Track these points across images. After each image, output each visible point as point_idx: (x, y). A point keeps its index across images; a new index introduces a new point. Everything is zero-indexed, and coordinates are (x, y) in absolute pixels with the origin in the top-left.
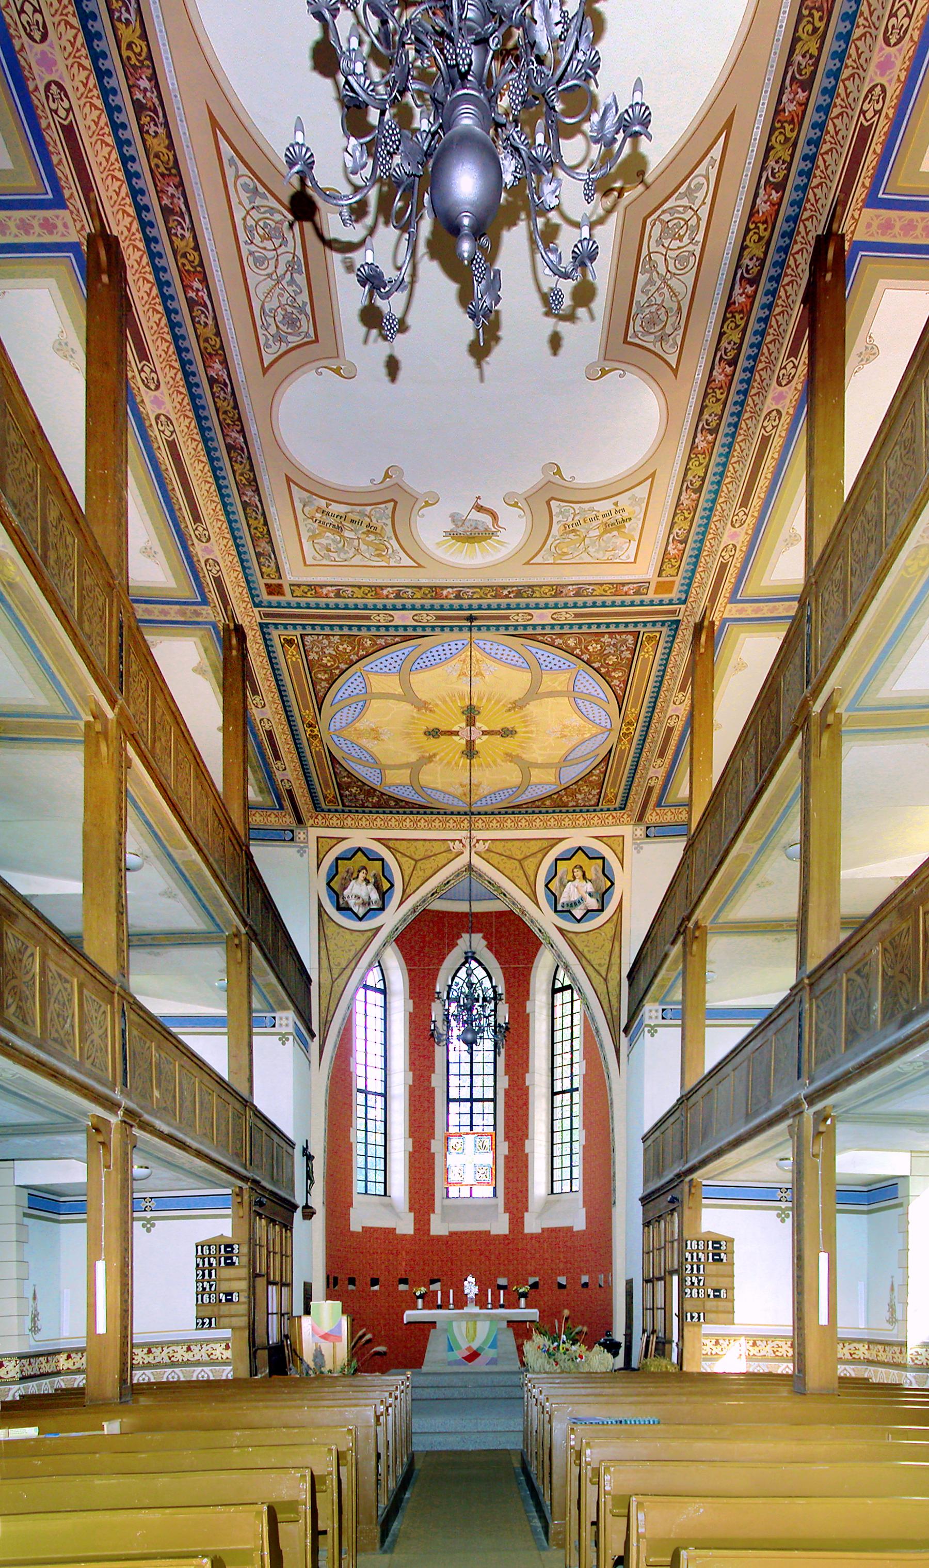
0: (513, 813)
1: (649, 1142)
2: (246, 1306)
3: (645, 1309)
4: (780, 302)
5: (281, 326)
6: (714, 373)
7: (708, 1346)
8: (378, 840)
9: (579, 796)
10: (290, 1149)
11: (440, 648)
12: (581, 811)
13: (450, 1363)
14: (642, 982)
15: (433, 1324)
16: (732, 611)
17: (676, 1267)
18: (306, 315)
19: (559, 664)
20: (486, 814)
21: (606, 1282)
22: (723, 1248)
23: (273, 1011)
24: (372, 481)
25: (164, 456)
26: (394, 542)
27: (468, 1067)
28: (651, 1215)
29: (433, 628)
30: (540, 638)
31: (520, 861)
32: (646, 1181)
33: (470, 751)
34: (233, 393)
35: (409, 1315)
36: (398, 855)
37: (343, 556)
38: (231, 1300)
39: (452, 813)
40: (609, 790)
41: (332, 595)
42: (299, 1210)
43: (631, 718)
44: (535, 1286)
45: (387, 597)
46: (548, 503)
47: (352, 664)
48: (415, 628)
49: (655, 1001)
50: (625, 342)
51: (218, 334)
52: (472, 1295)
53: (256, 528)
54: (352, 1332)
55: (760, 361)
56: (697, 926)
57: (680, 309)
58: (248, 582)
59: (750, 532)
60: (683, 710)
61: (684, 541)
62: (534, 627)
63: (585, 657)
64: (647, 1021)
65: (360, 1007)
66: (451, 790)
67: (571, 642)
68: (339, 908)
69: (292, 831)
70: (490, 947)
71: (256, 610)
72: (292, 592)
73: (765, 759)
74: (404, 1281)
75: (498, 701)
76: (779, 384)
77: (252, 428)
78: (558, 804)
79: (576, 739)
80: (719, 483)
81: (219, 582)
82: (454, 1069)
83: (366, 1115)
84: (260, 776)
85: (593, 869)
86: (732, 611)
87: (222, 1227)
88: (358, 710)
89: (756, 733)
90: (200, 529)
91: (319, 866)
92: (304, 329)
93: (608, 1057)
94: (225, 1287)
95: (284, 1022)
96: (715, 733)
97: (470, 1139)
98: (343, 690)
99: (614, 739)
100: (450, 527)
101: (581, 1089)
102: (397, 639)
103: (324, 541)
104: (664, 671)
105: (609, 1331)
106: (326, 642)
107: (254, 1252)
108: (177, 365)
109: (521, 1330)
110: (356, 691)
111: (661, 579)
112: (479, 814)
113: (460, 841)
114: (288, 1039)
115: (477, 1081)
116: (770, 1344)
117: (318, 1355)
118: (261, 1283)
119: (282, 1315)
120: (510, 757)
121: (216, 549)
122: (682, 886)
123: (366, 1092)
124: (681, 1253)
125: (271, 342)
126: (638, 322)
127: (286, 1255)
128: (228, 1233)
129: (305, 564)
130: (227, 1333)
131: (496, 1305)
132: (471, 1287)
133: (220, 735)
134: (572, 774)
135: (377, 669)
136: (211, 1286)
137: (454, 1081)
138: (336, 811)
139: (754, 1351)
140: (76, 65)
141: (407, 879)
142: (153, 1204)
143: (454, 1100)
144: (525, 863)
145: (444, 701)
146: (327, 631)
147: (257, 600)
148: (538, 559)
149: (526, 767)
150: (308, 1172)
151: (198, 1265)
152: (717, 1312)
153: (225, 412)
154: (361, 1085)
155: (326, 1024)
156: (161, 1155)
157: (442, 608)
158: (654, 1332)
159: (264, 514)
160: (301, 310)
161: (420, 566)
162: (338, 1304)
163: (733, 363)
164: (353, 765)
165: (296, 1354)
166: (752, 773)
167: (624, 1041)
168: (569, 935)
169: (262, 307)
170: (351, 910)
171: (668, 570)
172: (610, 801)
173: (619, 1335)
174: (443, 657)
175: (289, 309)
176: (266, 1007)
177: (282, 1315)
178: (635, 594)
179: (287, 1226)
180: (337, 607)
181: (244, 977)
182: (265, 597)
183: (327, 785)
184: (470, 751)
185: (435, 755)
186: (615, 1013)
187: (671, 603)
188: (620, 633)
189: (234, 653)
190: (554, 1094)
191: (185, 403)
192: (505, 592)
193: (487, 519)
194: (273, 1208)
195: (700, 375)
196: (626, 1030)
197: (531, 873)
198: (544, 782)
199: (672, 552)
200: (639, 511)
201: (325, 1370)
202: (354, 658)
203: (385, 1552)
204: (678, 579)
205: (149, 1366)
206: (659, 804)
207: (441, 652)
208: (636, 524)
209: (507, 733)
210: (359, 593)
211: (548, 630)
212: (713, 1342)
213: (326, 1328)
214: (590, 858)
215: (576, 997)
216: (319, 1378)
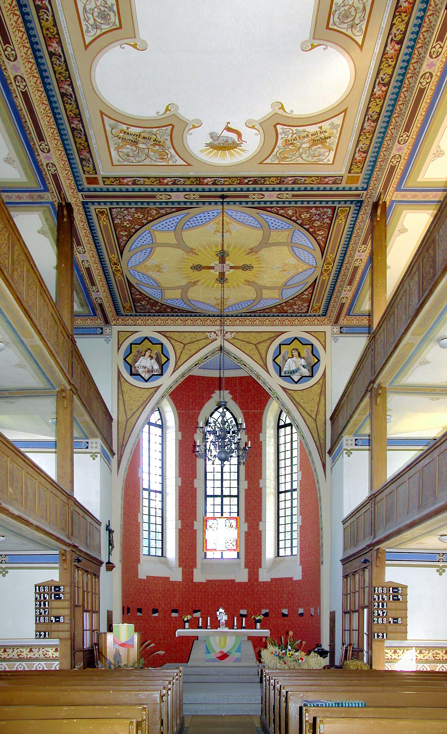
0: (250, 316)
1: (348, 524)
2: (69, 625)
3: (344, 630)
4: (431, 8)
5: (97, 19)
6: (387, 49)
7: (389, 654)
10: (98, 526)
11: (202, 215)
12: (296, 316)
13: (207, 661)
14: (341, 421)
15: (197, 638)
16: (398, 196)
17: (366, 603)
18: (114, 11)
19: (282, 226)
20: (232, 316)
21: (316, 612)
22: (400, 592)
23: (87, 438)
24: (157, 113)
25: (20, 102)
26: (172, 150)
27: (221, 475)
28: (349, 571)
29: (197, 203)
30: (270, 209)
31: (255, 345)
32: (345, 549)
33: (222, 278)
34: (65, 61)
35: (179, 632)
36: (172, 341)
37: (138, 159)
38: (59, 621)
39: (209, 316)
40: (314, 304)
41: (130, 183)
42: (104, 565)
43: (330, 260)
44: (266, 615)
45: (167, 184)
46: (275, 126)
47: (143, 225)
48: (185, 203)
49: (350, 434)
50: (327, 28)
51: (55, 25)
52: (223, 621)
53: (80, 144)
54: (142, 643)
55: (418, 43)
56: (380, 387)
57: (364, 9)
58: (74, 176)
59: (410, 147)
60: (365, 256)
61: (366, 152)
62: (265, 202)
63: (299, 222)
64: (345, 447)
65: (145, 436)
66: (209, 302)
67: (290, 212)
68: (131, 374)
69: (102, 329)
70: (234, 399)
71: (80, 194)
72: (104, 182)
73: (425, 283)
74: (175, 611)
75: (241, 248)
76: (431, 57)
77: (78, 83)
78: (282, 311)
79: (293, 273)
80: (389, 117)
81: (55, 177)
82: (209, 476)
83: (150, 505)
84: (81, 296)
85: (305, 351)
86: (398, 196)
87: (53, 575)
88: (147, 254)
89: (418, 268)
90: (22, 87)
91: (119, 349)
92: (113, 20)
93: (317, 470)
94: (55, 612)
95: (94, 445)
96: (388, 271)
97: (222, 521)
98: (137, 242)
99: (318, 273)
100: (209, 140)
101: (298, 490)
102: (174, 210)
103: (125, 150)
104: (352, 232)
105: (319, 645)
106: (126, 212)
107: (74, 591)
108: (28, 45)
109: (259, 644)
110: (145, 242)
111: (350, 175)
112: (227, 316)
113: (215, 332)
114: (97, 456)
115: (226, 484)
116: (431, 652)
117: (117, 655)
118: (79, 610)
119: (93, 631)
120: (249, 283)
121: (54, 157)
122: (368, 363)
123: (149, 490)
124: (371, 595)
125: (90, 29)
126: (336, 16)
127: (96, 593)
128: (57, 578)
129: (113, 165)
130: (56, 642)
132: (222, 616)
133: (55, 271)
134: (289, 294)
135: (160, 228)
136: (45, 612)
137: (209, 484)
138: (131, 315)
139: (420, 656)
140: (17, 31)
141: (178, 355)
142: (7, 559)
143: (235, 496)
144: (259, 346)
145: (205, 249)
146: (127, 206)
148: (268, 161)
149: (259, 289)
150: (109, 541)
151: (36, 598)
152: (395, 632)
153: (60, 73)
154: (146, 486)
155: (122, 447)
156: (12, 529)
157: (204, 190)
158: (350, 645)
159: (85, 135)
160: (111, 9)
161: (189, 165)
163: (400, 42)
164: (146, 289)
165: (102, 655)
166: (416, 292)
167: (328, 459)
168: (290, 392)
169: (85, 8)
170: (140, 375)
171: (355, 169)
172: (316, 310)
173: (326, 646)
174: (204, 221)
175: (103, 9)
176: (82, 436)
177: (93, 631)
178: (333, 183)
179: (97, 575)
180: (134, 191)
181: (68, 418)
182: (86, 186)
183: (125, 298)
184: (222, 278)
185: (198, 281)
186: (322, 441)
189: (65, 220)
190: (279, 493)
191: (47, 109)
192: (246, 181)
193: (235, 136)
194: (84, 563)
195: (378, 49)
196: (330, 452)
197: (263, 352)
198: (271, 298)
199: (358, 158)
200: (336, 133)
201: (122, 664)
202: (145, 222)
204: (362, 176)
206: (348, 314)
207: (203, 218)
208: (334, 141)
209: (246, 268)
210: (148, 181)
211: (275, 205)
212: (393, 651)
213: (123, 639)
214: (303, 344)
216: (118, 670)
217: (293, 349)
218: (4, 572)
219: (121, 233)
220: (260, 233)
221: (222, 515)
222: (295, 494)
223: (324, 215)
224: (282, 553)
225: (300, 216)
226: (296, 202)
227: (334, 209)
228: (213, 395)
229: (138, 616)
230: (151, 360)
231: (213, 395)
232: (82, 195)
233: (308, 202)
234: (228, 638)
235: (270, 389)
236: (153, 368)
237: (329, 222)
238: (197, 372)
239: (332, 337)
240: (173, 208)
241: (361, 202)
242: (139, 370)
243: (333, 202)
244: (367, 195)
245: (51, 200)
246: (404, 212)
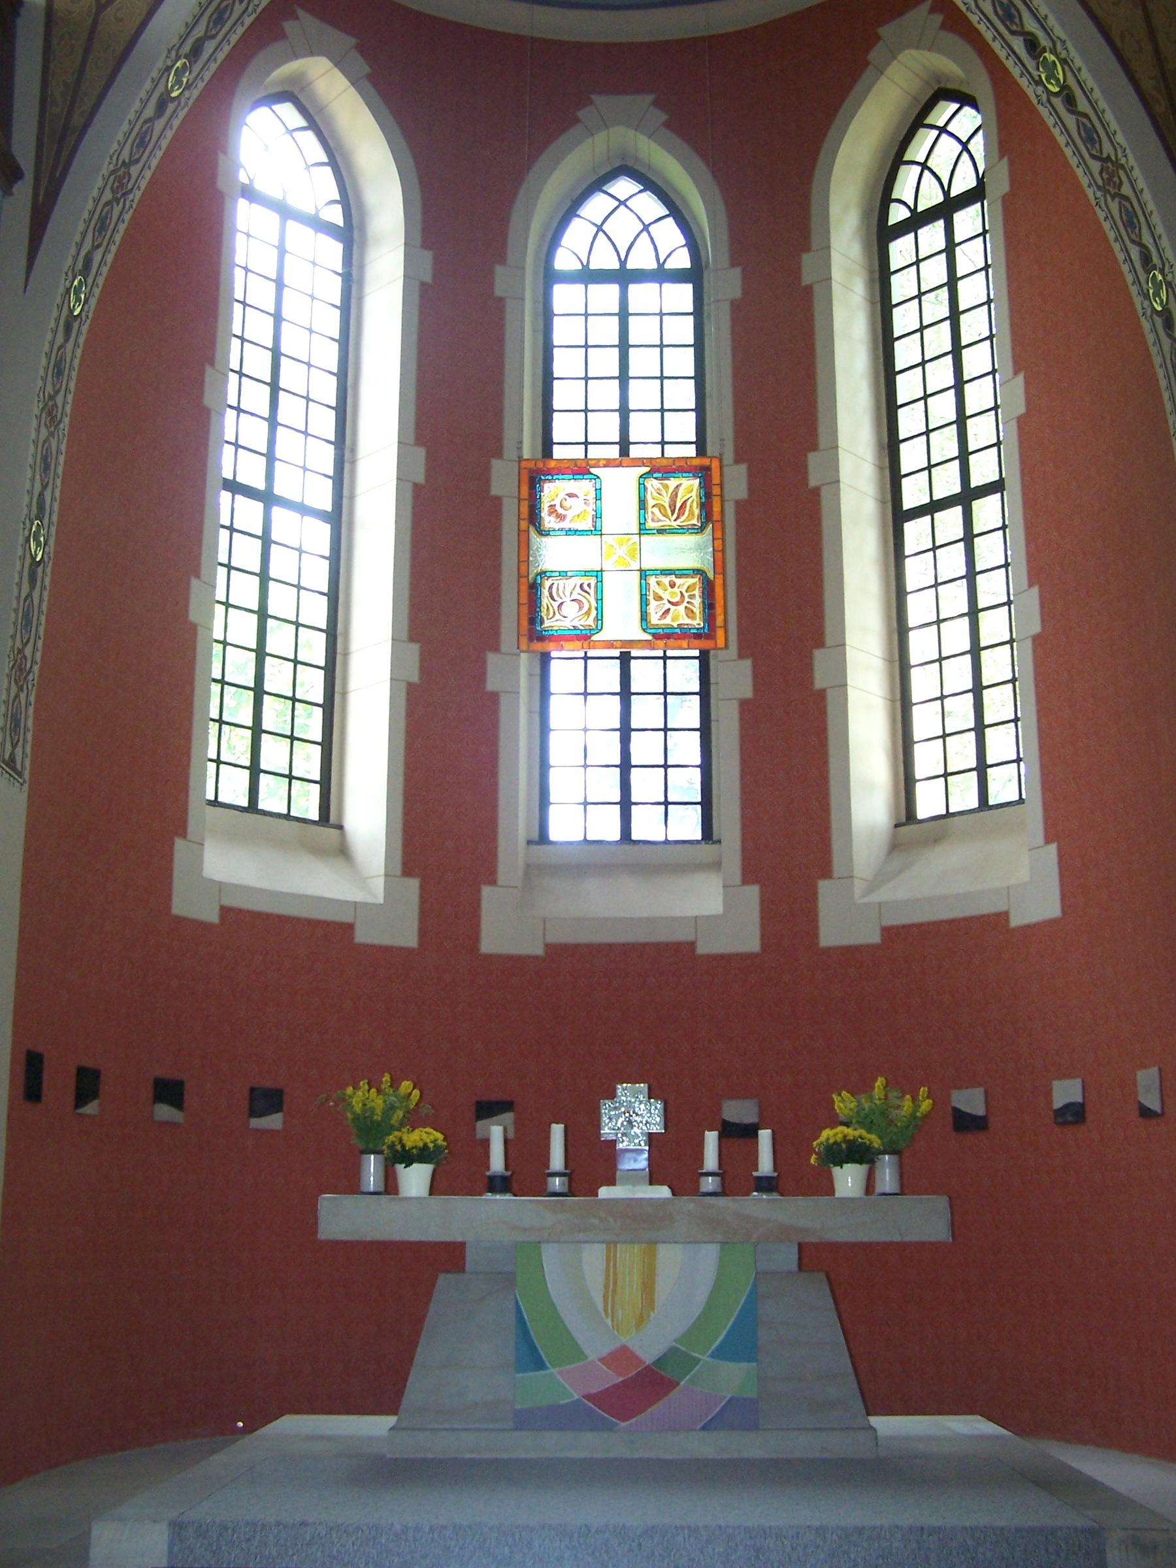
13: (525, 1420)
15: (450, 1256)
131: (737, 1178)
132: (633, 1118)
221: (624, 452)
222: (987, 511)
224: (929, 803)
229: (163, 1124)
234: (670, 1257)
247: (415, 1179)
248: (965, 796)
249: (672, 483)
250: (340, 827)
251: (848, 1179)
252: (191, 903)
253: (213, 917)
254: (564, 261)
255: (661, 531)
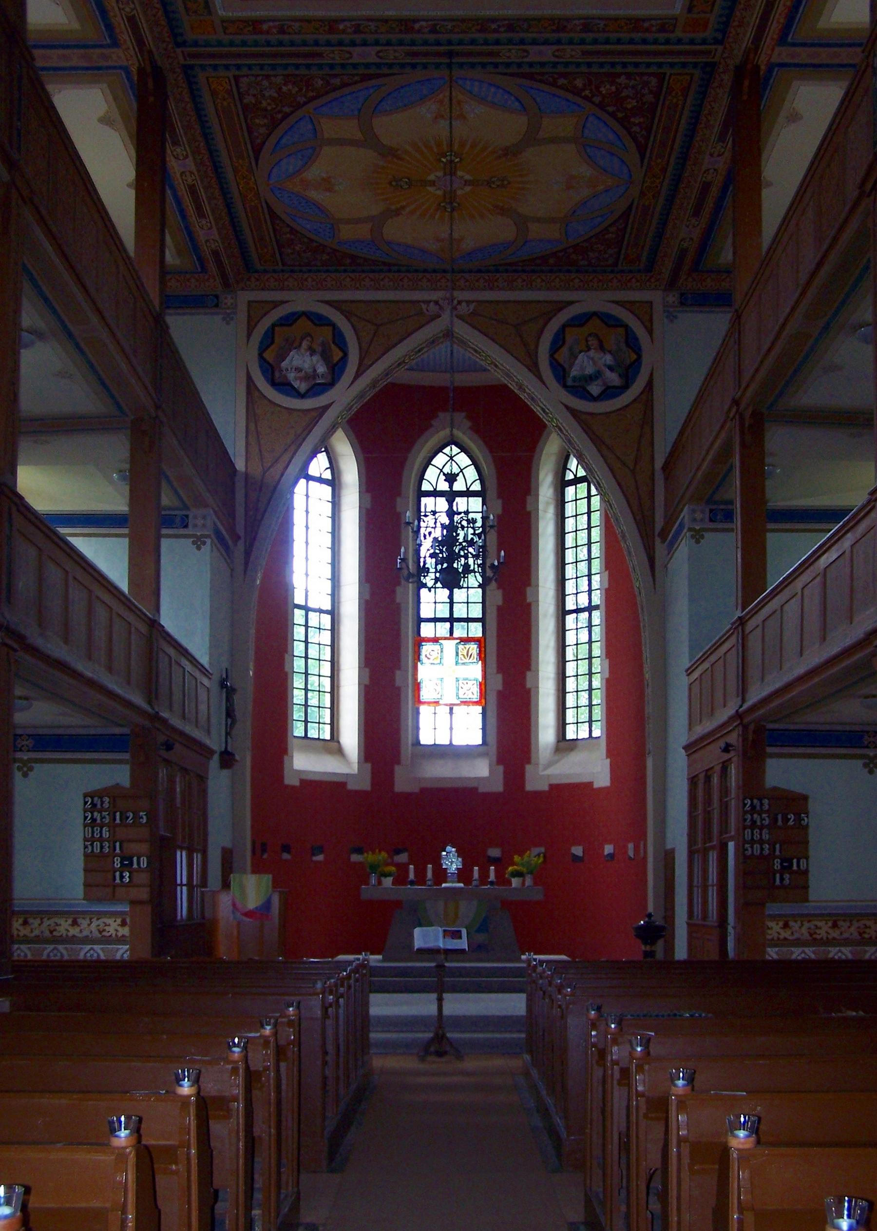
1: (696, 675)
8: (328, 303)
9: (591, 254)
16: (782, 54)
20: (470, 271)
23: (187, 508)
29: (403, 66)
41: (275, 31)
47: (300, 106)
48: (378, 66)
62: (531, 65)
67: (579, 83)
68: (274, 384)
69: (217, 297)
71: (179, 50)
72: (225, 30)
85: (613, 338)
86: (782, 54)
95: (200, 522)
96: (765, 193)
101: (603, 607)
106: (265, 83)
114: (204, 543)
116: (856, 924)
123: (306, 609)
133: (132, 193)
138: (274, 271)
147: (180, 39)
162: (267, 879)
167: (660, 549)
176: (177, 503)
187: (704, 42)
188: (642, 75)
192: (494, 26)
203: (332, 1171)
205: (26, 940)
215: (594, 491)
217: (590, 335)
218: (25, 769)
219: (257, 121)
220: (524, 119)
223: (643, 88)
224: (570, 734)
225: (598, 88)
226: (589, 65)
227: (661, 77)
228: (433, 422)
230: (311, 355)
231: (433, 422)
232: (183, 52)
233: (613, 65)
235: (544, 411)
236: (315, 371)
237: (653, 100)
238: (403, 377)
239: (664, 311)
240: (353, 75)
241: (713, 65)
242: (288, 375)
243: (660, 65)
244: (723, 52)
245: (125, 64)
246: (795, 83)
247: (388, 882)
248: (584, 734)
249: (467, 646)
250: (339, 742)
251: (515, 882)
252: (290, 780)
253: (297, 783)
254: (426, 487)
255: (463, 664)
